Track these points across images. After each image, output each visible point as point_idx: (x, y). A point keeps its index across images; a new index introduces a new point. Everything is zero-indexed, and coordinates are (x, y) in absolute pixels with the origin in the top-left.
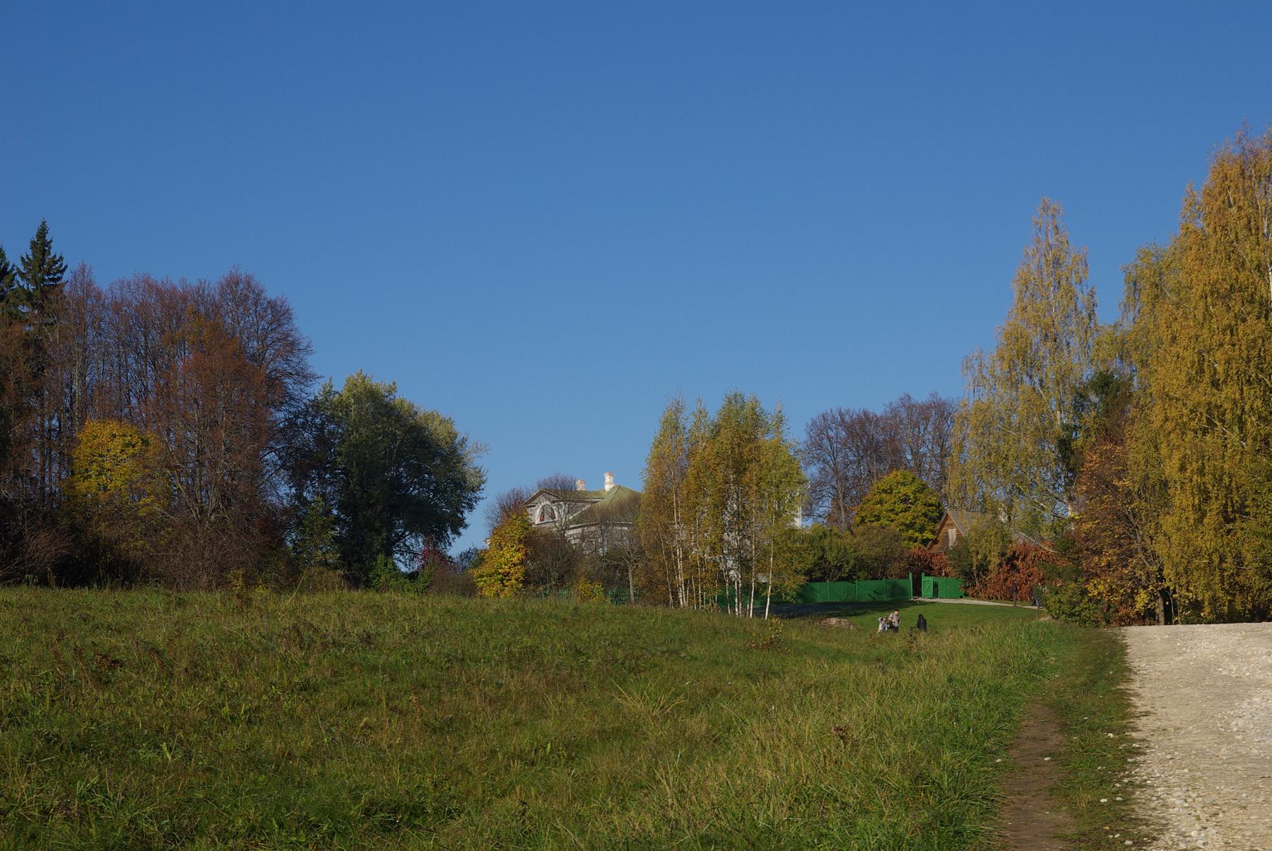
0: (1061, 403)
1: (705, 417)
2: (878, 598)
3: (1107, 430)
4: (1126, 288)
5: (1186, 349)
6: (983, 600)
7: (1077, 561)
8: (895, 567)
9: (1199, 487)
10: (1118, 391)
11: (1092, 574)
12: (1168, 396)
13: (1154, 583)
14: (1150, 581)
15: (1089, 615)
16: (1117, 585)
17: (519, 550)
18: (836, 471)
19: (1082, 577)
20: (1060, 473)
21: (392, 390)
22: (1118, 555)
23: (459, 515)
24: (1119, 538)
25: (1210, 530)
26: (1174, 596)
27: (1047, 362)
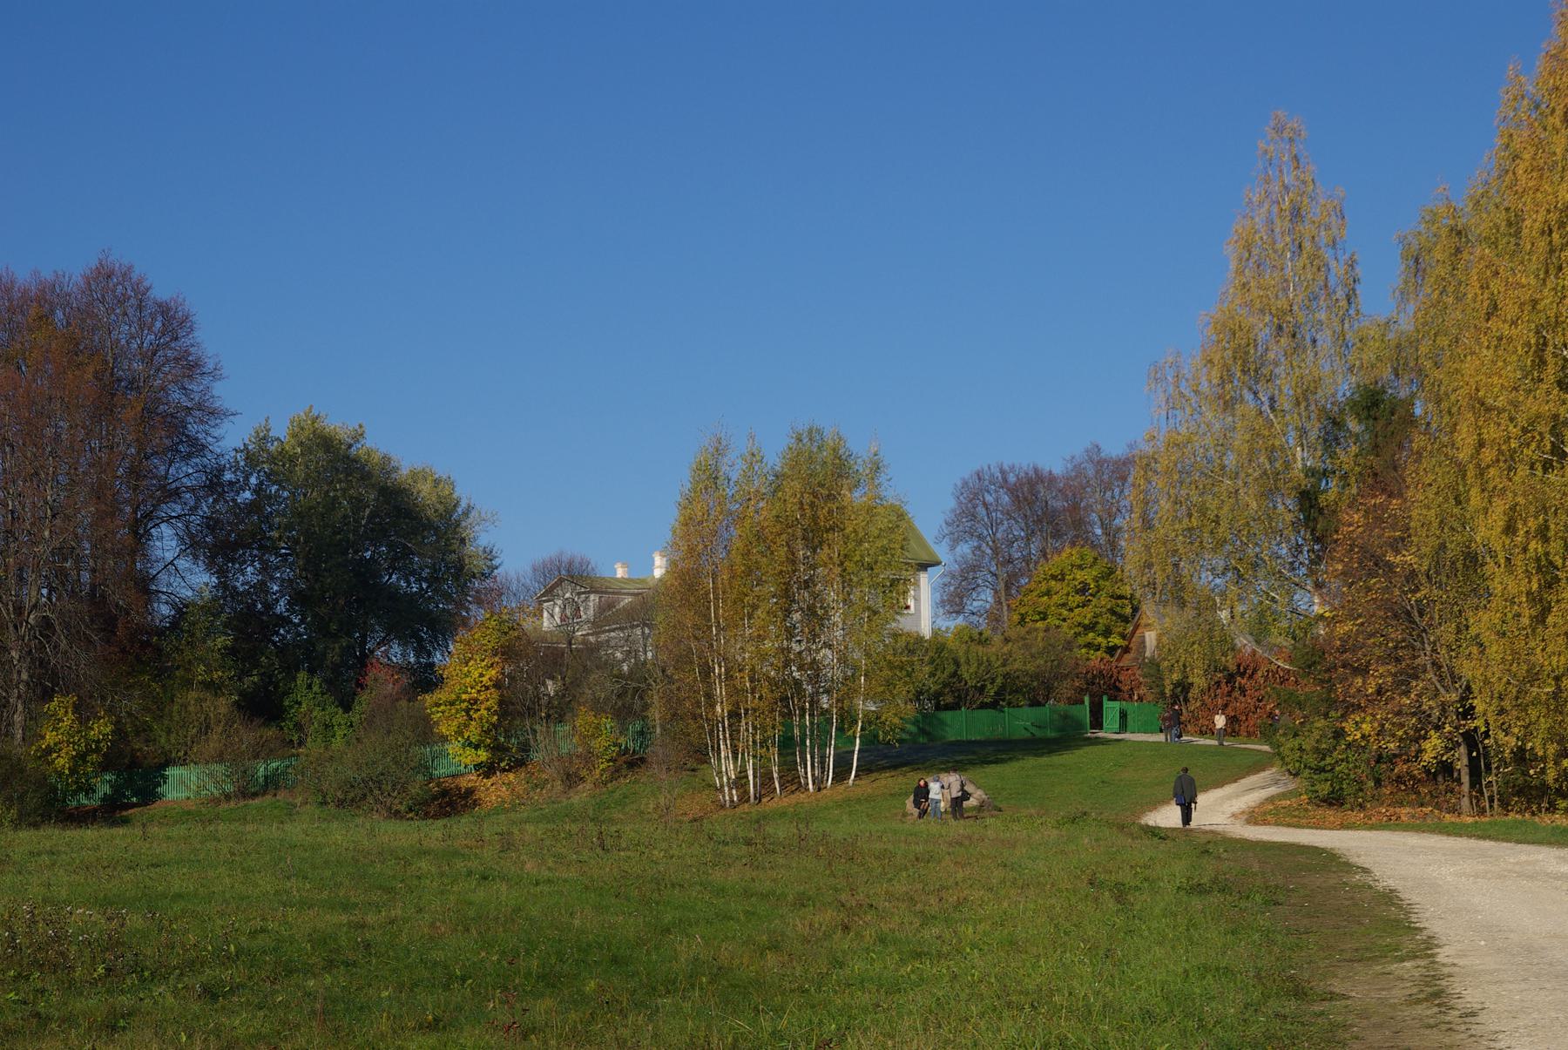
0: (1303, 432)
1: (761, 461)
2: (1038, 733)
3: (1376, 475)
4: (1403, 267)
5: (1514, 323)
6: (1192, 735)
7: (1328, 684)
8: (1066, 688)
9: (1538, 560)
10: (1393, 415)
11: (1353, 706)
12: (1483, 404)
13: (1452, 721)
14: (1446, 718)
15: (1346, 771)
16: (1393, 724)
17: (492, 665)
18: (996, 551)
19: (1337, 710)
20: (1302, 545)
21: (358, 436)
22: (1395, 675)
23: (464, 614)
24: (1396, 648)
25: (1559, 635)
26: (1486, 741)
27: (1279, 370)
